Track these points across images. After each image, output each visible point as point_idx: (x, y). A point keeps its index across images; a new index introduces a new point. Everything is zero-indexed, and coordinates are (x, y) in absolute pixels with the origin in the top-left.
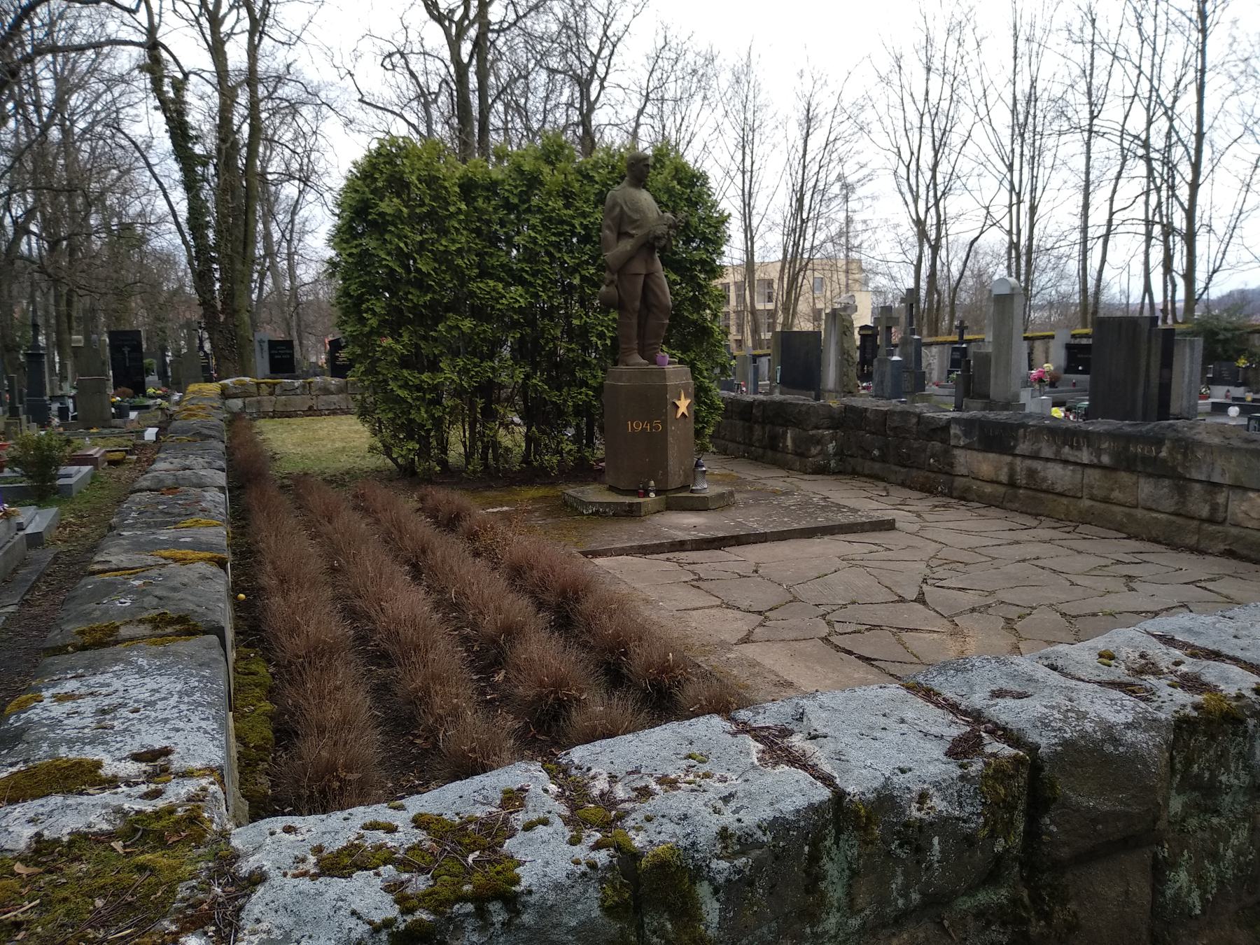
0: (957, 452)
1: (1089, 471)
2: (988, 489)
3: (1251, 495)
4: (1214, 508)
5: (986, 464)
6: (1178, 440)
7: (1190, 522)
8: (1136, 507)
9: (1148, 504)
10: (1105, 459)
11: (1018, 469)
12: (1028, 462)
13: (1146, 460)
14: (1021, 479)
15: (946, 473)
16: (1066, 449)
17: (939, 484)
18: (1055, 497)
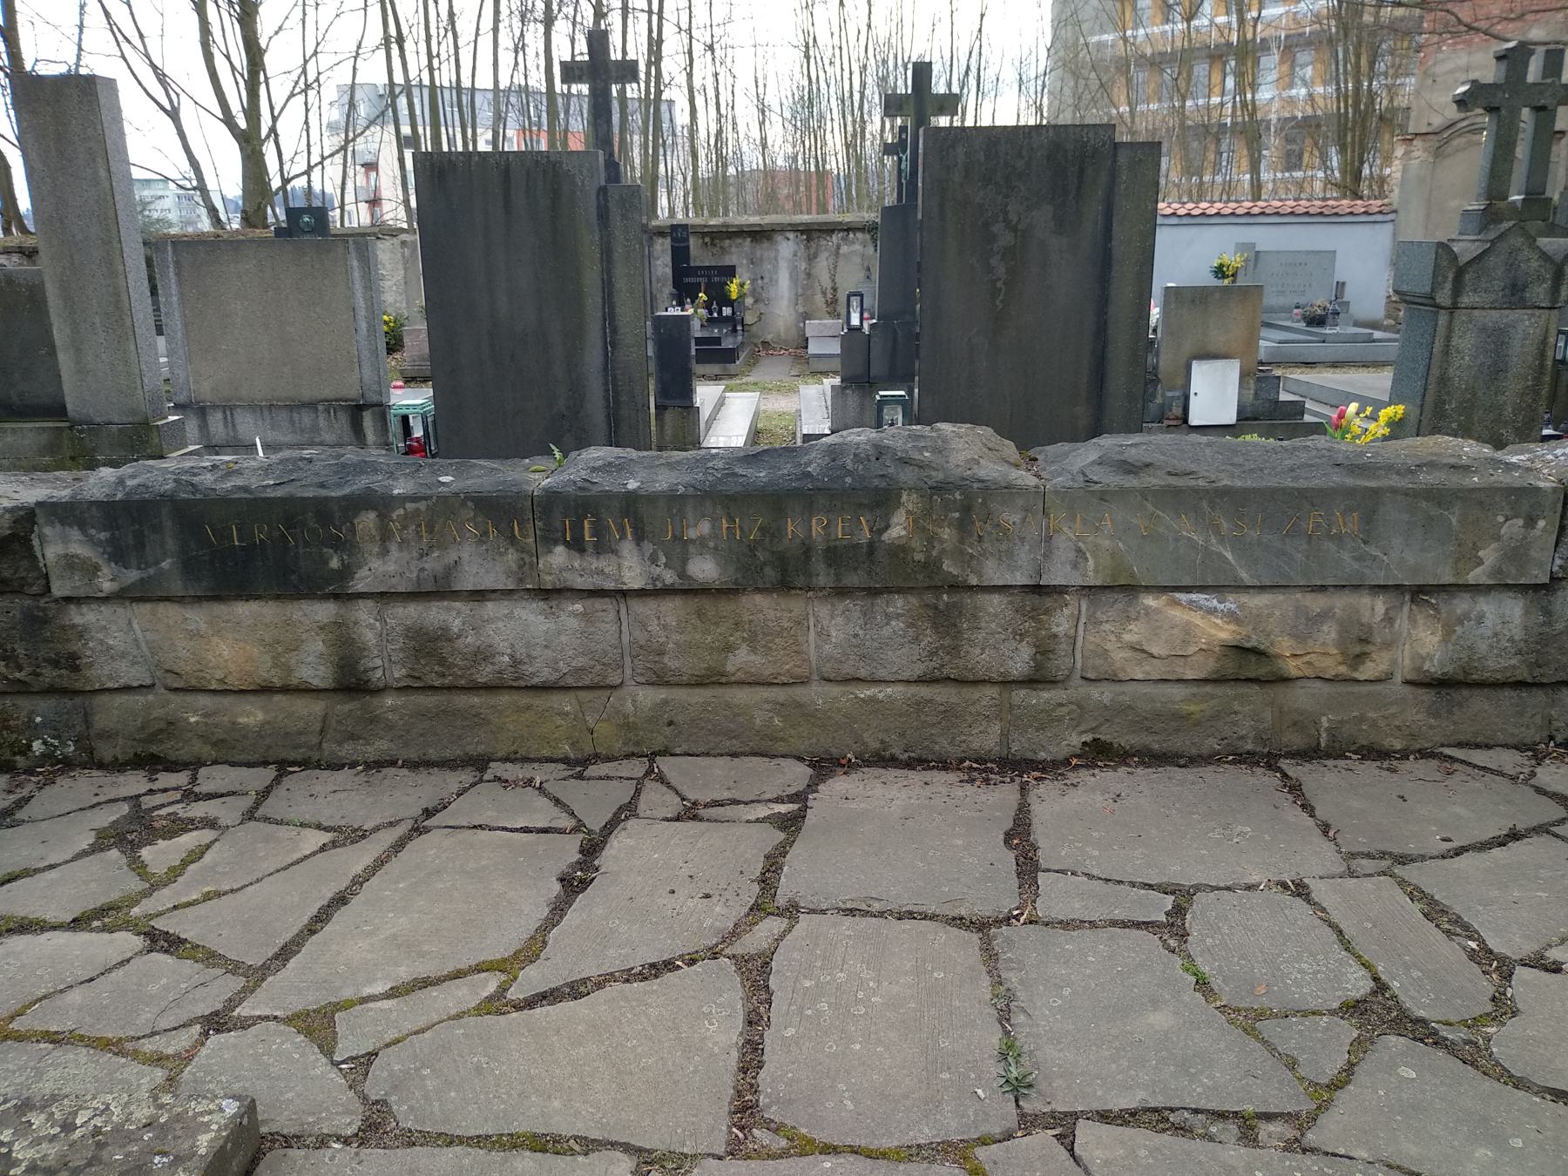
0: (82, 617)
1: (642, 608)
2: (252, 714)
3: (1150, 601)
4: (1043, 651)
5: (232, 640)
6: (940, 488)
7: (974, 693)
8: (803, 682)
9: (847, 669)
10: (704, 569)
11: (369, 637)
12: (411, 613)
13: (836, 556)
14: (385, 664)
15: (51, 691)
16: (559, 556)
17: (33, 730)
18: (524, 699)
